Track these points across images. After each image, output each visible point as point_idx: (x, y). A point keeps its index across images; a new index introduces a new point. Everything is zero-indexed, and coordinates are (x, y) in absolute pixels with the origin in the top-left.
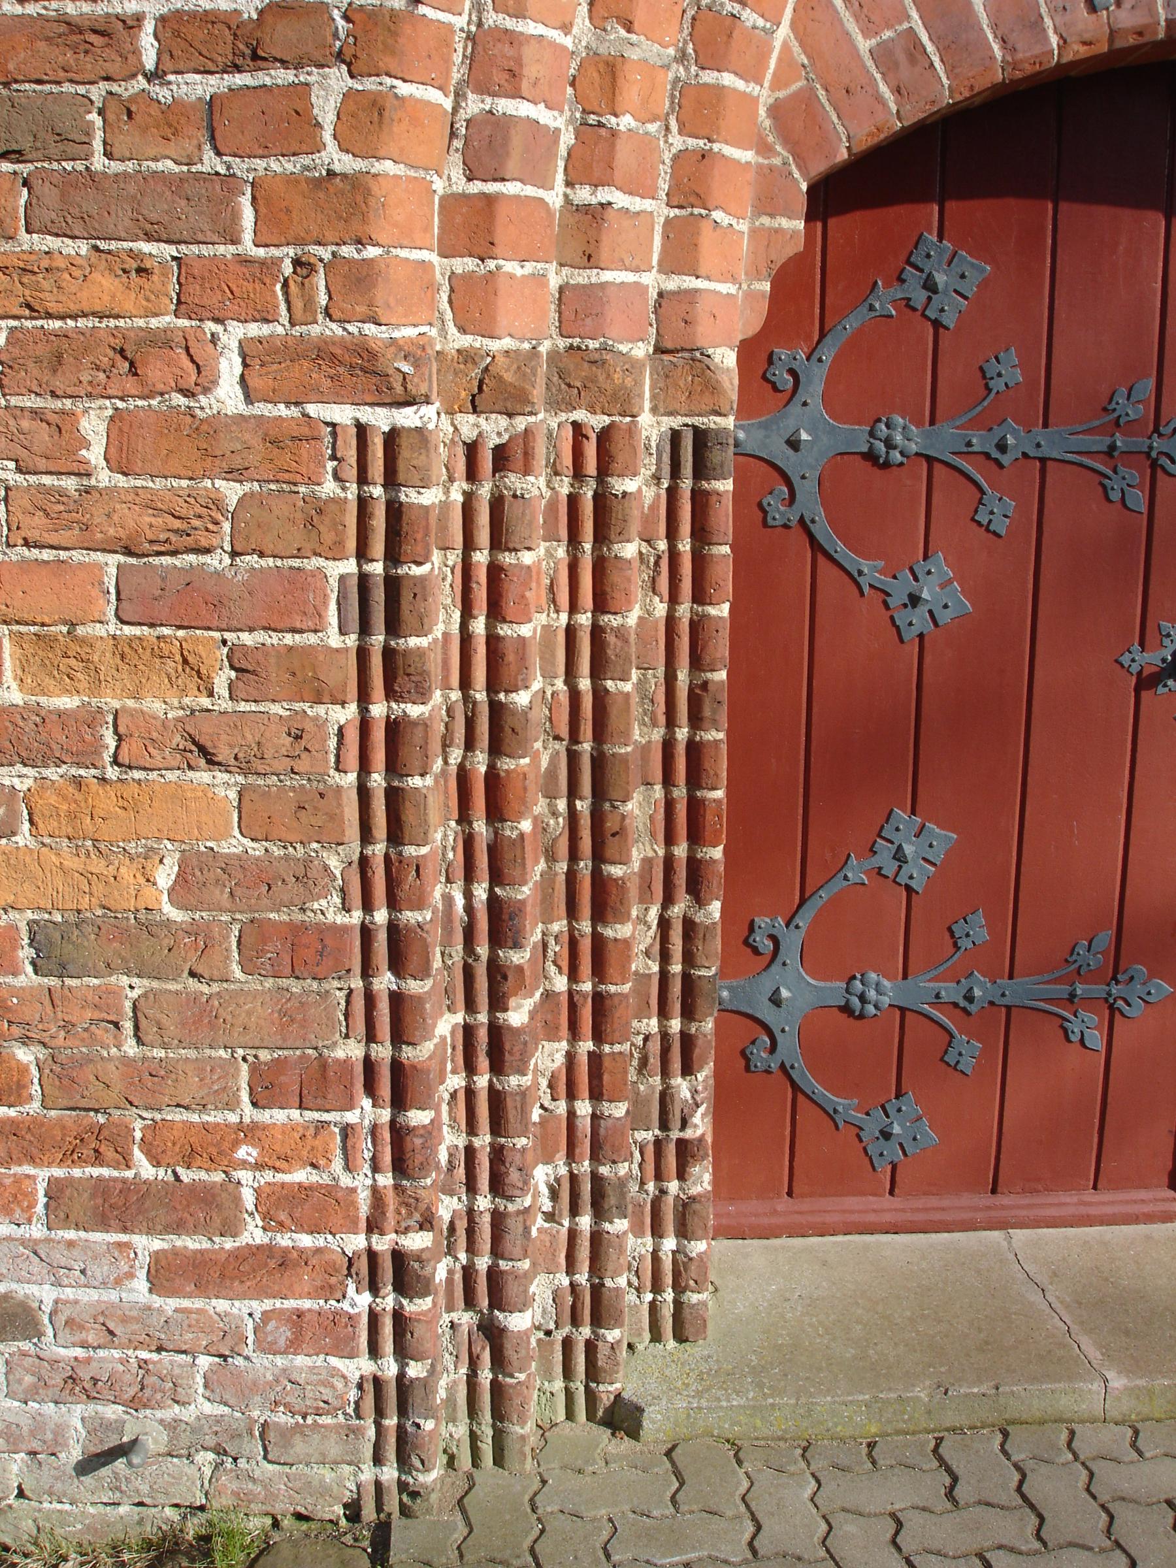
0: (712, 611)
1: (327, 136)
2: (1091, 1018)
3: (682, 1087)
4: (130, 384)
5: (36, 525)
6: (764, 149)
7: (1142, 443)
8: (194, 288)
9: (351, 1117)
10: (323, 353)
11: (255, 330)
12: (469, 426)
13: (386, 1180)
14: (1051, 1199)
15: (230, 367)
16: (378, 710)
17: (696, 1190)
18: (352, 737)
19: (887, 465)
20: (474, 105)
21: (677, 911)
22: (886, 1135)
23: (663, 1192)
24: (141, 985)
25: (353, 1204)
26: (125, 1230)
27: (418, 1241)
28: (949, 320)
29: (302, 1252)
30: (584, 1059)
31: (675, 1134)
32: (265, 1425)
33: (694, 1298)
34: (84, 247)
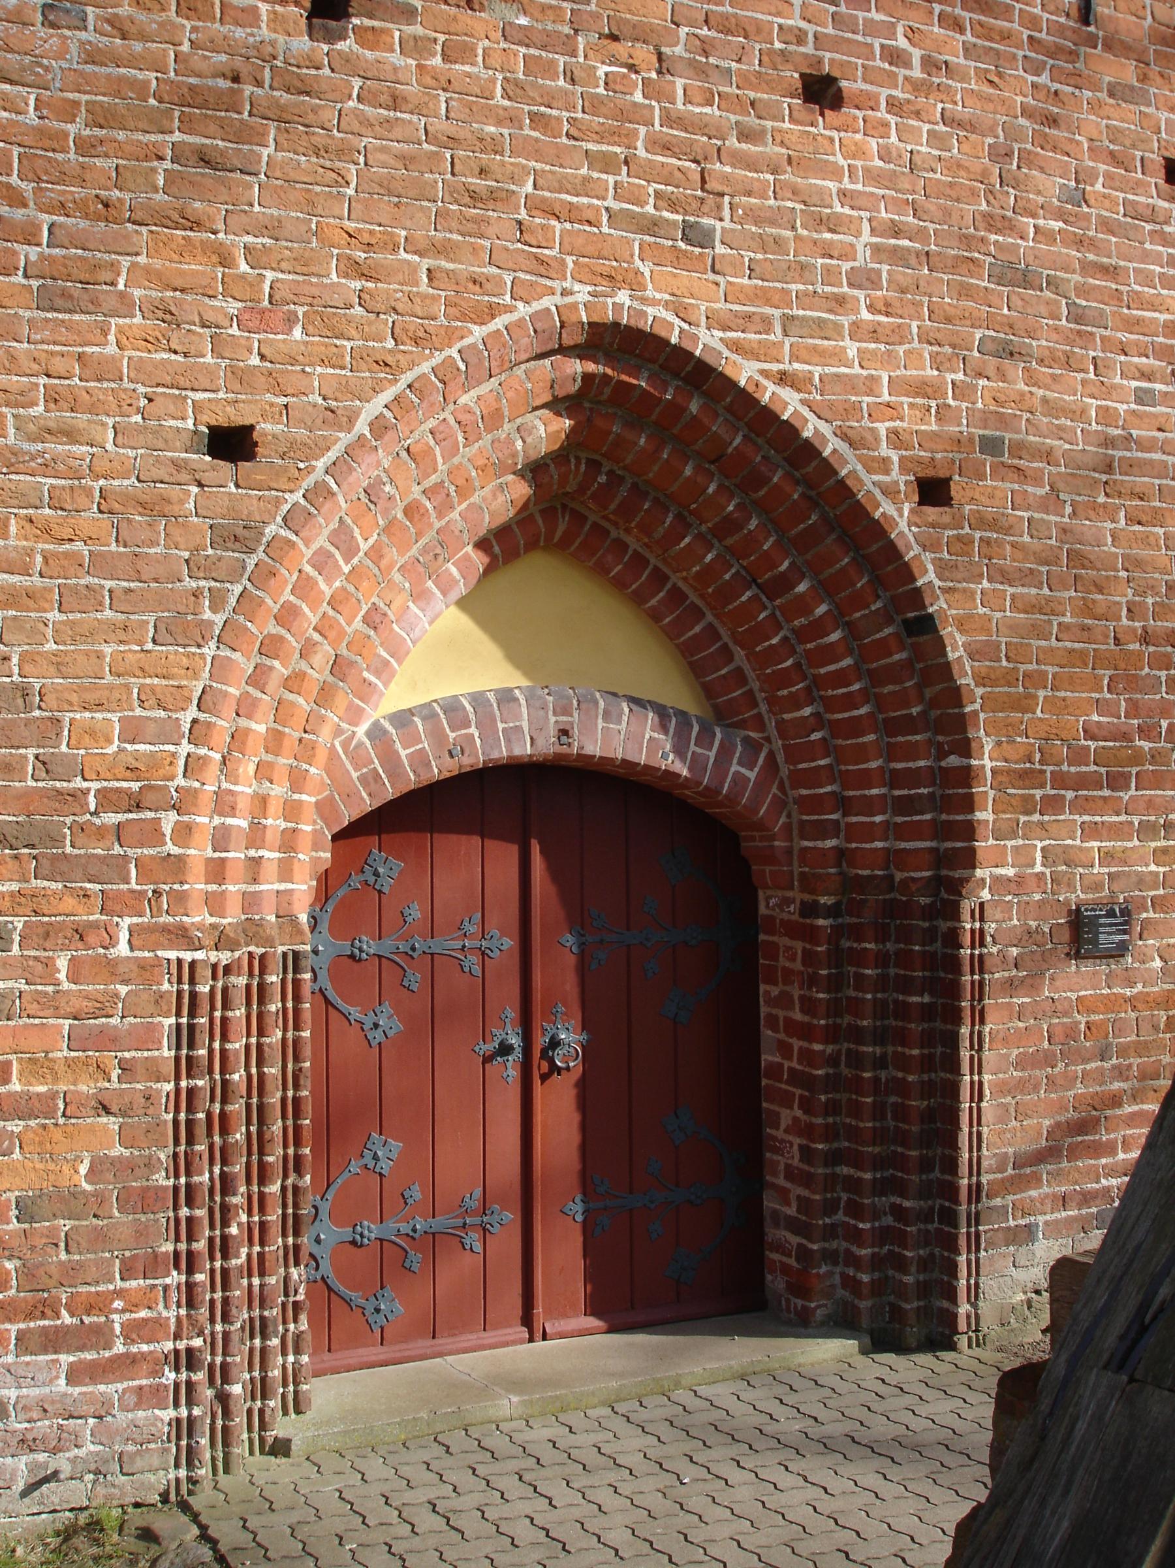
0: (303, 1034)
1: (168, 839)
2: (475, 1236)
3: (294, 1273)
4: (80, 945)
5: (33, 1008)
6: (315, 822)
7: (477, 944)
8: (109, 903)
9: (168, 1281)
10: (165, 929)
11: (135, 920)
12: (213, 956)
13: (183, 1312)
14: (463, 1337)
15: (124, 936)
16: (183, 1084)
17: (303, 1328)
18: (172, 1096)
19: (360, 960)
20: (217, 820)
21: (290, 1181)
22: (378, 1310)
23: (287, 1330)
24: (69, 1224)
25: (168, 1326)
26: (56, 1352)
27: (198, 1342)
28: (386, 890)
29: (142, 1354)
30: (255, 1256)
31: (291, 1299)
32: (121, 1454)
33: (305, 1387)
34: (60, 886)
